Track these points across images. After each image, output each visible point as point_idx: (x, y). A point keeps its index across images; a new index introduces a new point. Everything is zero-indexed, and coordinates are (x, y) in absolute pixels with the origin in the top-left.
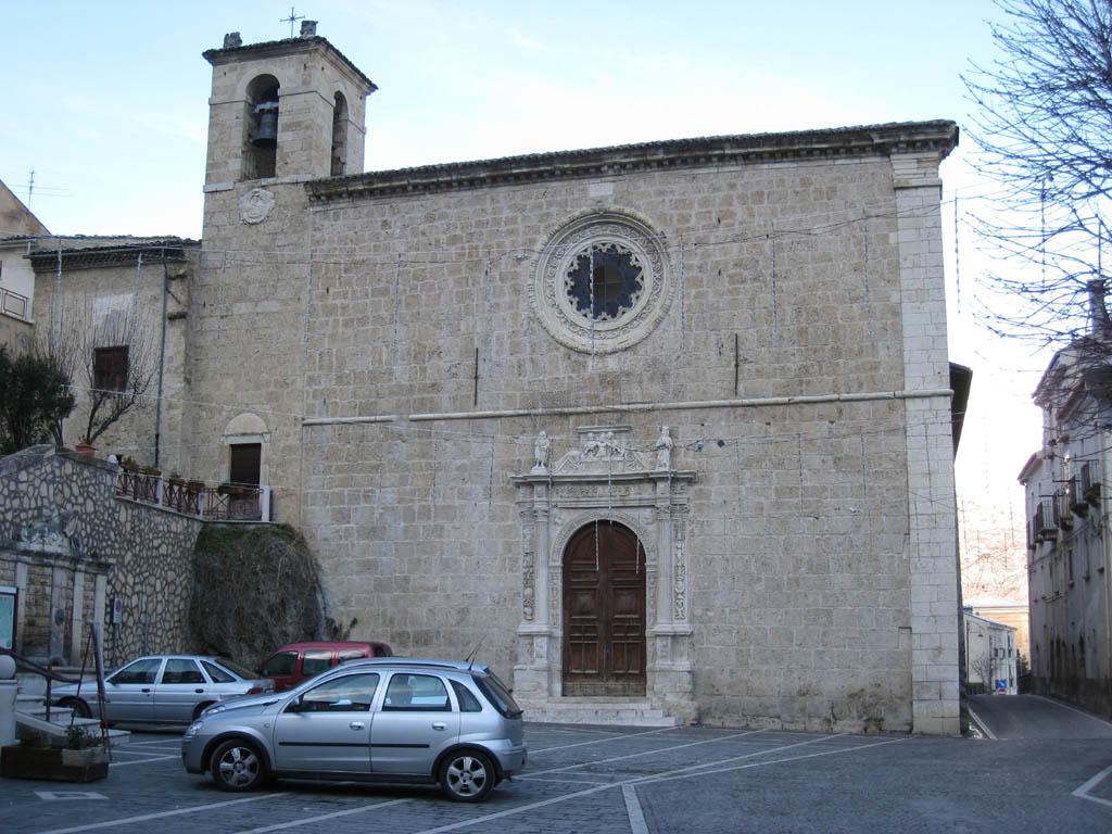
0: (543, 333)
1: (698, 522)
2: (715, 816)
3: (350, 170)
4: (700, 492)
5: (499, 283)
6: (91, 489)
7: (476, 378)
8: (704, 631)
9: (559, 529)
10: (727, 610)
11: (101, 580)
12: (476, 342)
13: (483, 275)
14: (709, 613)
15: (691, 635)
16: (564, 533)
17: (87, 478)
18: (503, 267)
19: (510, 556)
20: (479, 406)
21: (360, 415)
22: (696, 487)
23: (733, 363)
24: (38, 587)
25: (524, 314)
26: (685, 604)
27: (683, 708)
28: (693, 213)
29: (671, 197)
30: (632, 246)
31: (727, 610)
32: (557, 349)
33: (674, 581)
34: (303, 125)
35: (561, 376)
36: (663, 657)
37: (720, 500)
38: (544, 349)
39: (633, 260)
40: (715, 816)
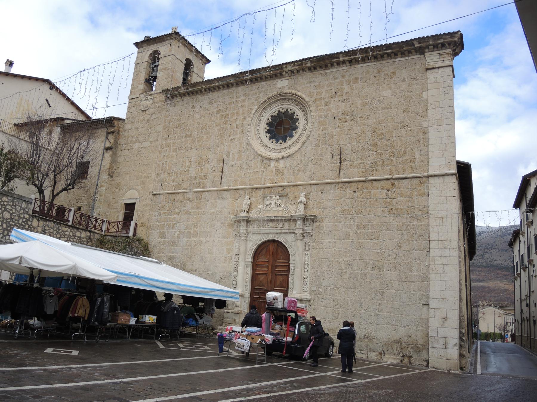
1: (317, 242)
6: (8, 207)
7: (222, 172)
8: (317, 299)
10: (329, 288)
16: (253, 245)
17: (6, 201)
21: (175, 190)
22: (317, 224)
31: (329, 288)
33: (303, 271)
34: (167, 69)
39: (274, 114)
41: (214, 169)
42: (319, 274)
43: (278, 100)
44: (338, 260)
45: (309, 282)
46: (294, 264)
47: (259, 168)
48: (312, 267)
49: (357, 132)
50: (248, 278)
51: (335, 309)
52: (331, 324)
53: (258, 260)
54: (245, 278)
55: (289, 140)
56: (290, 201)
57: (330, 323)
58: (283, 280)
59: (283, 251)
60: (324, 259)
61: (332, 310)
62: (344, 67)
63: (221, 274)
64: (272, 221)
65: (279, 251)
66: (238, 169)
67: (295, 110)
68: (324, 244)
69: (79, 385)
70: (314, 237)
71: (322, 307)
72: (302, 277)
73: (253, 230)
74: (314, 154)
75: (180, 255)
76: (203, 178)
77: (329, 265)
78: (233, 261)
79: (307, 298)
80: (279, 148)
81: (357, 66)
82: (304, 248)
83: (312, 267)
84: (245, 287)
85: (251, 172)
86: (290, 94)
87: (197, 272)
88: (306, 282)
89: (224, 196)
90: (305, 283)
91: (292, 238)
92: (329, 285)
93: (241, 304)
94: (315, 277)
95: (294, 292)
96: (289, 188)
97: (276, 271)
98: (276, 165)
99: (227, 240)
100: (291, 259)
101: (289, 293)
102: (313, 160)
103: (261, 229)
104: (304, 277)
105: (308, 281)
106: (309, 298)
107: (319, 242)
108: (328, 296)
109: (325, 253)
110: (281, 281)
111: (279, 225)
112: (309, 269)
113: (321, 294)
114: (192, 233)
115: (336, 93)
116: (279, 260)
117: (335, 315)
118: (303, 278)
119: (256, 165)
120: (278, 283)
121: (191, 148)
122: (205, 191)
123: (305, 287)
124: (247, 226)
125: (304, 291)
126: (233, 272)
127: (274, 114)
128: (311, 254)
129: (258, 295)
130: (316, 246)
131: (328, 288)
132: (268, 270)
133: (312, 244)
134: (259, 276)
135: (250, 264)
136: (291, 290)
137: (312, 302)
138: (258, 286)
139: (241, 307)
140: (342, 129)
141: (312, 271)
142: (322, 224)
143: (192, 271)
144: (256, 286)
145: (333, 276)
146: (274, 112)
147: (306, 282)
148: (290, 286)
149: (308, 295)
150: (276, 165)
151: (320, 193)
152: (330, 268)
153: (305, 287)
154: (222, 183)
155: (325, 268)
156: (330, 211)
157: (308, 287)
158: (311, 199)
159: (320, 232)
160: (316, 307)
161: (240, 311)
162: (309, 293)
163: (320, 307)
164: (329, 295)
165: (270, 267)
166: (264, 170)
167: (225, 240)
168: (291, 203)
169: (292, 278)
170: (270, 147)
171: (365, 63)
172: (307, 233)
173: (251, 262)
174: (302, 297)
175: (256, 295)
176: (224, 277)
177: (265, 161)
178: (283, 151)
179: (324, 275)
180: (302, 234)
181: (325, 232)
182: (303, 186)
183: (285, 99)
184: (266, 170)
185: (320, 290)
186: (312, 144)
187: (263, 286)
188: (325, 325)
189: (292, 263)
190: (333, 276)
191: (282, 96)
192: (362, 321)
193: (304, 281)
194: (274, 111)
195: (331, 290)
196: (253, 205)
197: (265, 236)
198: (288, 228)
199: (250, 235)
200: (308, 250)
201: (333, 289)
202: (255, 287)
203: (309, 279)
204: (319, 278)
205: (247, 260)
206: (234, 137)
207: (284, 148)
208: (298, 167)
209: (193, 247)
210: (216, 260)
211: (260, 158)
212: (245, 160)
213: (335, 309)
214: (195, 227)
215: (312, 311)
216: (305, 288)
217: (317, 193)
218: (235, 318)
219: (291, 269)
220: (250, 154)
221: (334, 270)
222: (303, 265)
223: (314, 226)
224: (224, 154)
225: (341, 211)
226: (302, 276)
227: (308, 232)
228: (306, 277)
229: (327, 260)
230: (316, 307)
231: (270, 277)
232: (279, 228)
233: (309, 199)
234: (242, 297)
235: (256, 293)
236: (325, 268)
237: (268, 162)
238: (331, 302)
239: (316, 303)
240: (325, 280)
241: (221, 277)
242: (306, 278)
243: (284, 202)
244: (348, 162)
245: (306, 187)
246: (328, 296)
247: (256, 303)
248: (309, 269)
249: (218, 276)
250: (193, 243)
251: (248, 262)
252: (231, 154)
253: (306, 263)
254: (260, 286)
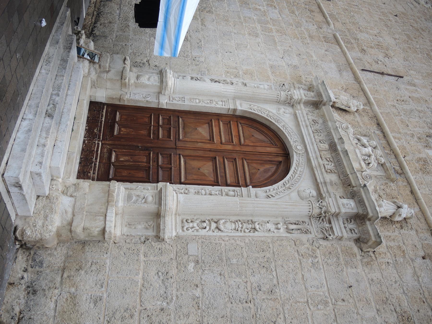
1: (313, 251)
4: (348, 253)
8: (165, 258)
9: (274, 111)
10: (198, 293)
11: (180, 216)
14: (192, 265)
15: (158, 238)
16: (271, 114)
19: (241, 73)
20: (361, 72)
22: (356, 249)
24: (190, 52)
26: (203, 232)
27: (46, 217)
29: (47, 312)
31: (198, 293)
33: (234, 219)
36: (129, 197)
37: (352, 281)
41: (379, 62)
42: (234, 261)
44: (282, 316)
45: (209, 236)
46: (249, 196)
48: (247, 241)
50: (199, 102)
51: (136, 314)
52: (92, 305)
53: (240, 125)
54: (200, 98)
56: (382, 187)
57: (95, 303)
58: (205, 175)
59: (270, 174)
60: (274, 273)
61: (135, 308)
63: (202, 59)
64: (333, 147)
65: (267, 166)
68: (313, 271)
69: (80, 163)
70: (323, 243)
71: (140, 276)
72: (218, 217)
73: (302, 113)
75: (227, 9)
76: (360, 48)
77: (263, 289)
78: (231, 79)
79: (167, 230)
82: (293, 220)
83: (247, 241)
84: (181, 96)
85: (402, 117)
87: (200, 26)
88: (208, 228)
89: (344, 73)
90: (205, 225)
91: (308, 191)
92: (206, 293)
93: (145, 86)
94: (223, 250)
95: (180, 196)
96: (405, 184)
97: (221, 160)
99: (270, 72)
100: (260, 191)
101: (175, 186)
103: (309, 127)
104: (222, 222)
105: (210, 233)
106: (166, 237)
107: (316, 257)
108: (174, 292)
109: (291, 276)
110: (201, 170)
111: (327, 163)
112: (242, 234)
113: (179, 271)
114: (268, 26)
116: (248, 165)
117: (118, 315)
118: (215, 218)
119: (418, 125)
120: (195, 164)
121: (395, 39)
122: (341, 47)
123: (195, 225)
124: (307, 103)
125: (182, 222)
126: (210, 78)
128: (280, 239)
129: (163, 123)
130: (302, 249)
131: (199, 290)
132: (221, 143)
133: (304, 237)
134: (206, 126)
135: (232, 107)
136: (182, 191)
137: (156, 245)
138: (184, 124)
139: (137, 85)
141: (238, 242)
142: (360, 262)
143: (202, 20)
144: (183, 120)
145: (234, 305)
147: (208, 228)
148: (193, 188)
149: (174, 234)
151: (422, 254)
152: (254, 292)
153: (195, 225)
154: (364, 72)
155: (253, 279)
156: (396, 282)
157: (196, 233)
158: (402, 231)
159: (338, 258)
160: (142, 257)
161: (127, 80)
162: (178, 237)
163: (142, 267)
164: (179, 293)
165: (229, 147)
167: (269, 69)
168: (378, 188)
169: (213, 192)
172: (328, 225)
173: (235, 110)
174: (167, 218)
175: (163, 119)
176: (197, 63)
179: (234, 275)
180: (325, 213)
181: (344, 273)
182: (420, 213)
185: (191, 266)
187: (185, 134)
188: (88, 287)
189: (249, 191)
190: (234, 305)
192: (131, 297)
193: (209, 221)
195: (195, 298)
196: (347, 116)
197: (296, 137)
198: (328, 180)
199: (290, 110)
200: (288, 231)
201: (196, 306)
202: (181, 119)
203: (215, 234)
204: (222, 261)
205: (238, 102)
209: (244, 24)
210: (228, 53)
212: (417, 108)
213: (136, 314)
214: (278, 31)
215: (128, 246)
216: (191, 225)
217: (419, 246)
218: (113, 71)
219: (234, 191)
221: (252, 306)
222: (250, 218)
223: (348, 243)
225: (405, 312)
226: (222, 217)
227: (331, 228)
228: (222, 227)
229: (275, 282)
230: (142, 257)
231: (208, 146)
232: (321, 162)
233: (402, 227)
234: (157, 90)
235: (169, 120)
236: (253, 279)
238: (159, 303)
239: (152, 258)
240: (219, 279)
241: (197, 59)
242: (217, 228)
243: (376, 173)
245: (423, 220)
246: (174, 292)
247: (147, 120)
248: (242, 234)
249: (197, 54)
250: (251, 25)
251: (235, 104)
253: (257, 227)
254: (184, 128)
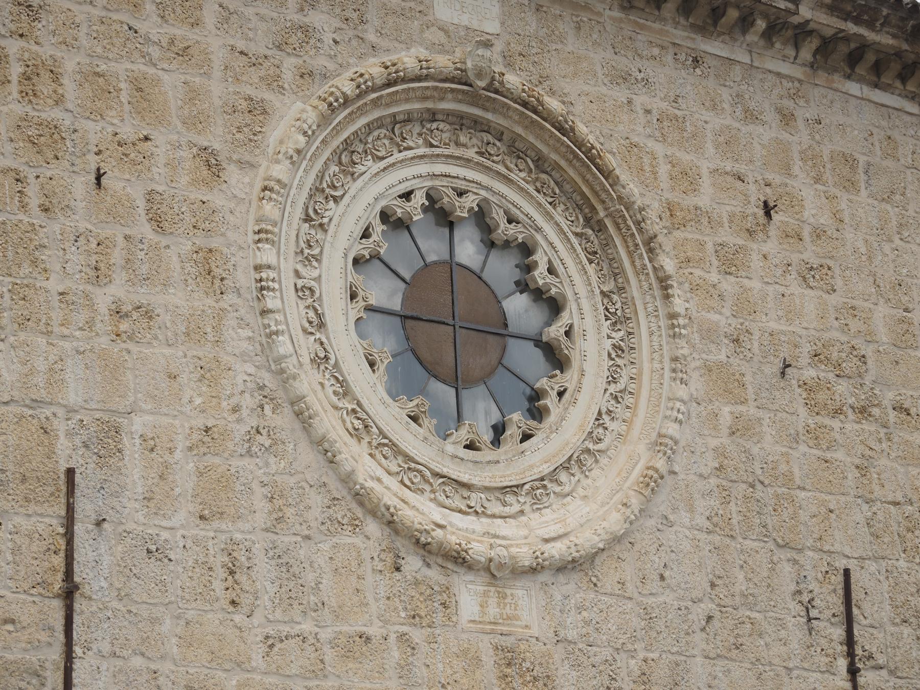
0: (307, 456)
2: (370, 467)
3: (483, 387)
5: (146, 230)
7: (69, 593)
12: (63, 445)
13: (81, 185)
18: (159, 170)
23: (842, 664)
25: (243, 372)
28: (705, 167)
30: (540, 221)
32: (355, 526)
35: (374, 630)
38: (315, 515)
39: (542, 268)
40: (370, 467)
43: (433, 116)
47: (373, 607)
49: (899, 498)
55: (526, 437)
62: (785, 58)
66: (208, 585)
67: (539, 230)
74: (713, 585)
80: (475, 481)
81: (839, 81)
86: (525, 104)
98: (493, 610)
102: (716, 623)
115: (768, 210)
127: (542, 268)
140: (828, 455)
146: (557, 263)
150: (493, 610)
166: (417, 635)
170: (412, 452)
171: (876, 86)
177: (412, 563)
178: (495, 507)
183: (477, 125)
184: (432, 640)
186: (691, 509)
191: (474, 99)
194: (560, 269)
206: (142, 295)
207: (504, 489)
208: (632, 654)
211: (372, 527)
220: (292, 481)
224: (60, 427)
237: (434, 574)
244: (884, 673)
252: (132, 447)
